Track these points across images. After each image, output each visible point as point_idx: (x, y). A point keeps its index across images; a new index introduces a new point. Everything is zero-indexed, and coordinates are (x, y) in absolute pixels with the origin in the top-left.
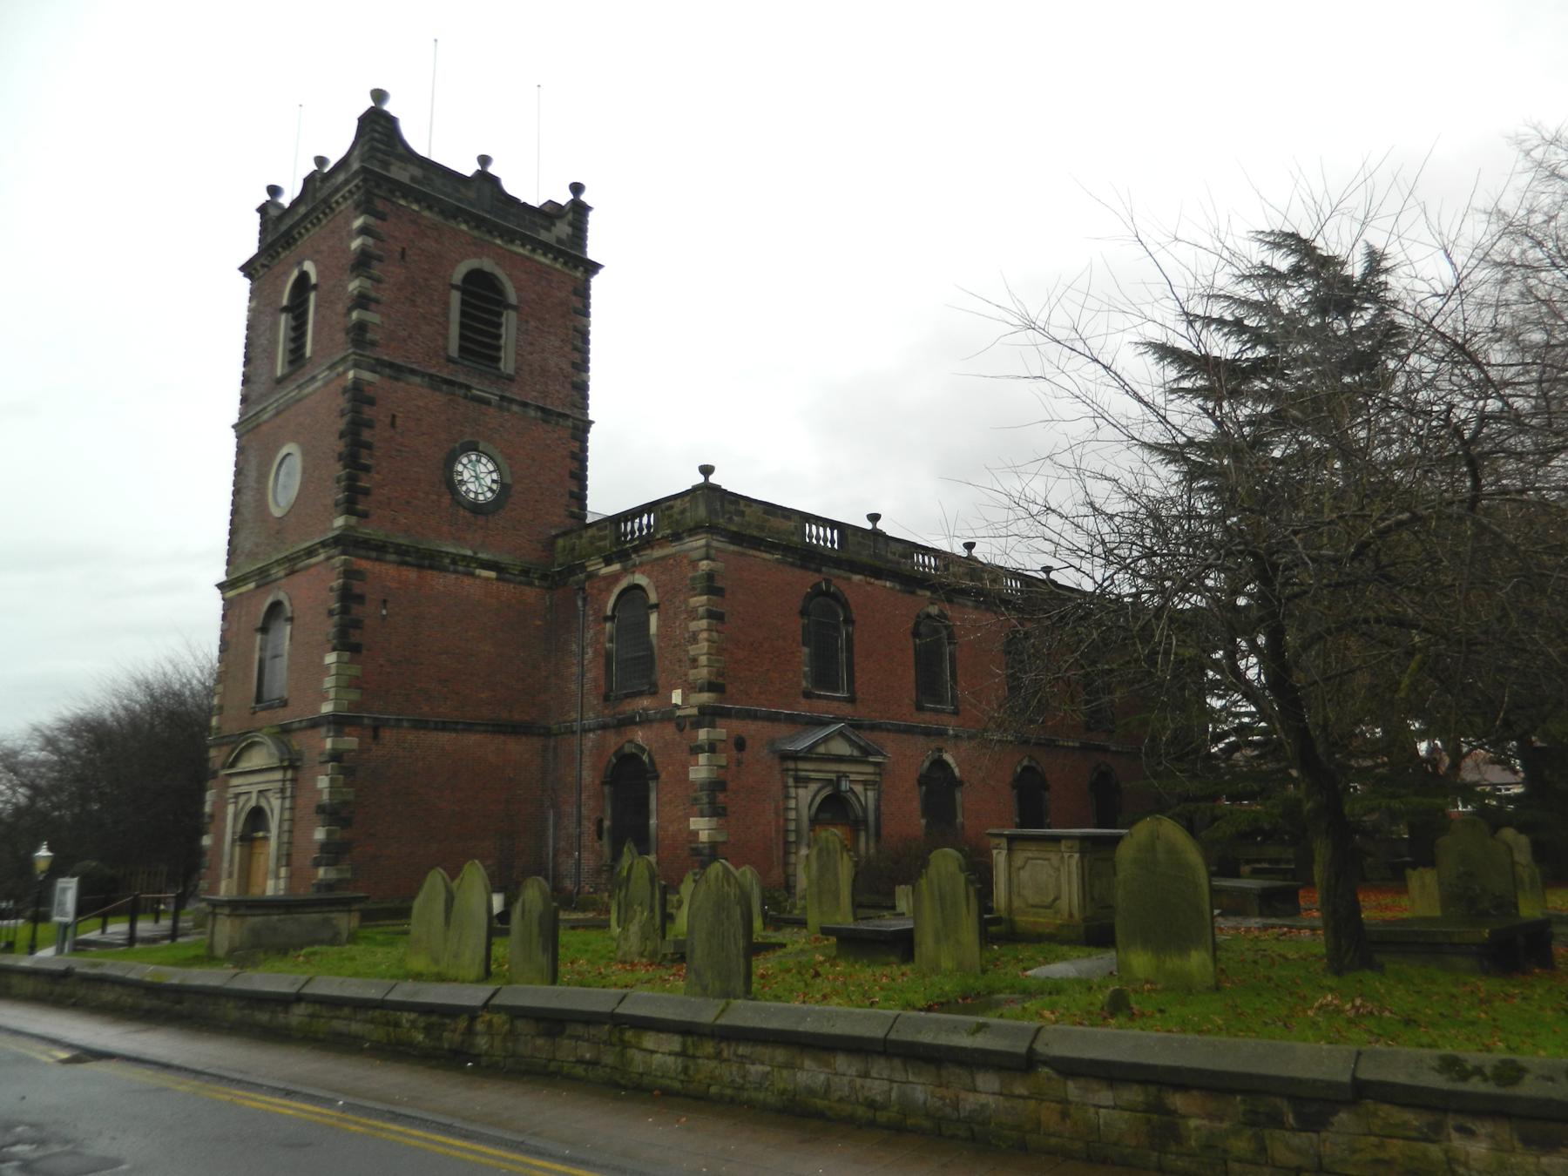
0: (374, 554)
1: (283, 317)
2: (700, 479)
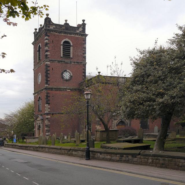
0: (51, 90)
1: (38, 52)
2: (98, 74)
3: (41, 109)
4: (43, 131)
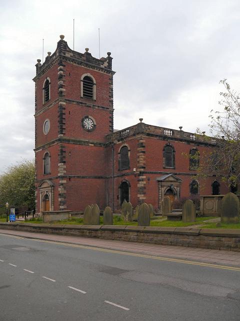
0: (67, 142)
2: (140, 122)
3: (49, 170)
4: (53, 203)
